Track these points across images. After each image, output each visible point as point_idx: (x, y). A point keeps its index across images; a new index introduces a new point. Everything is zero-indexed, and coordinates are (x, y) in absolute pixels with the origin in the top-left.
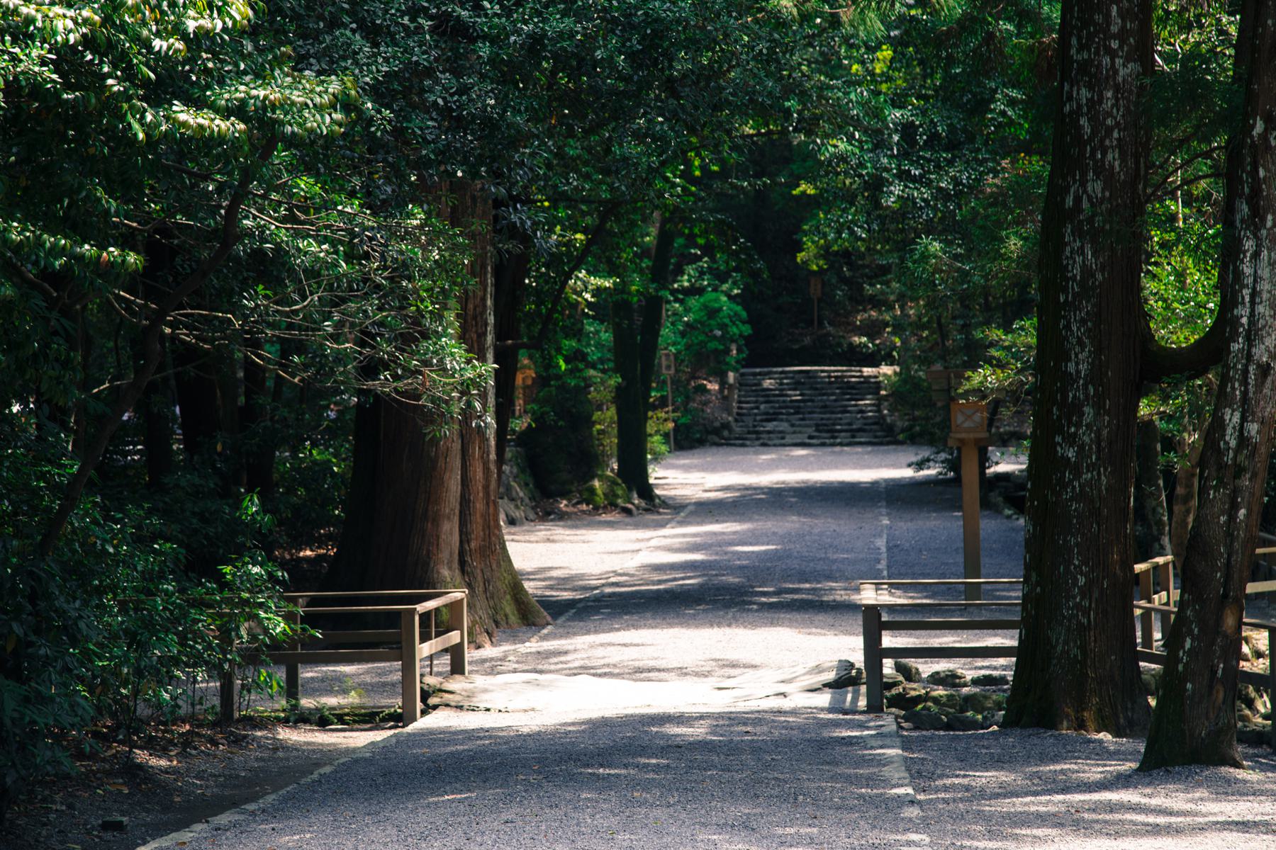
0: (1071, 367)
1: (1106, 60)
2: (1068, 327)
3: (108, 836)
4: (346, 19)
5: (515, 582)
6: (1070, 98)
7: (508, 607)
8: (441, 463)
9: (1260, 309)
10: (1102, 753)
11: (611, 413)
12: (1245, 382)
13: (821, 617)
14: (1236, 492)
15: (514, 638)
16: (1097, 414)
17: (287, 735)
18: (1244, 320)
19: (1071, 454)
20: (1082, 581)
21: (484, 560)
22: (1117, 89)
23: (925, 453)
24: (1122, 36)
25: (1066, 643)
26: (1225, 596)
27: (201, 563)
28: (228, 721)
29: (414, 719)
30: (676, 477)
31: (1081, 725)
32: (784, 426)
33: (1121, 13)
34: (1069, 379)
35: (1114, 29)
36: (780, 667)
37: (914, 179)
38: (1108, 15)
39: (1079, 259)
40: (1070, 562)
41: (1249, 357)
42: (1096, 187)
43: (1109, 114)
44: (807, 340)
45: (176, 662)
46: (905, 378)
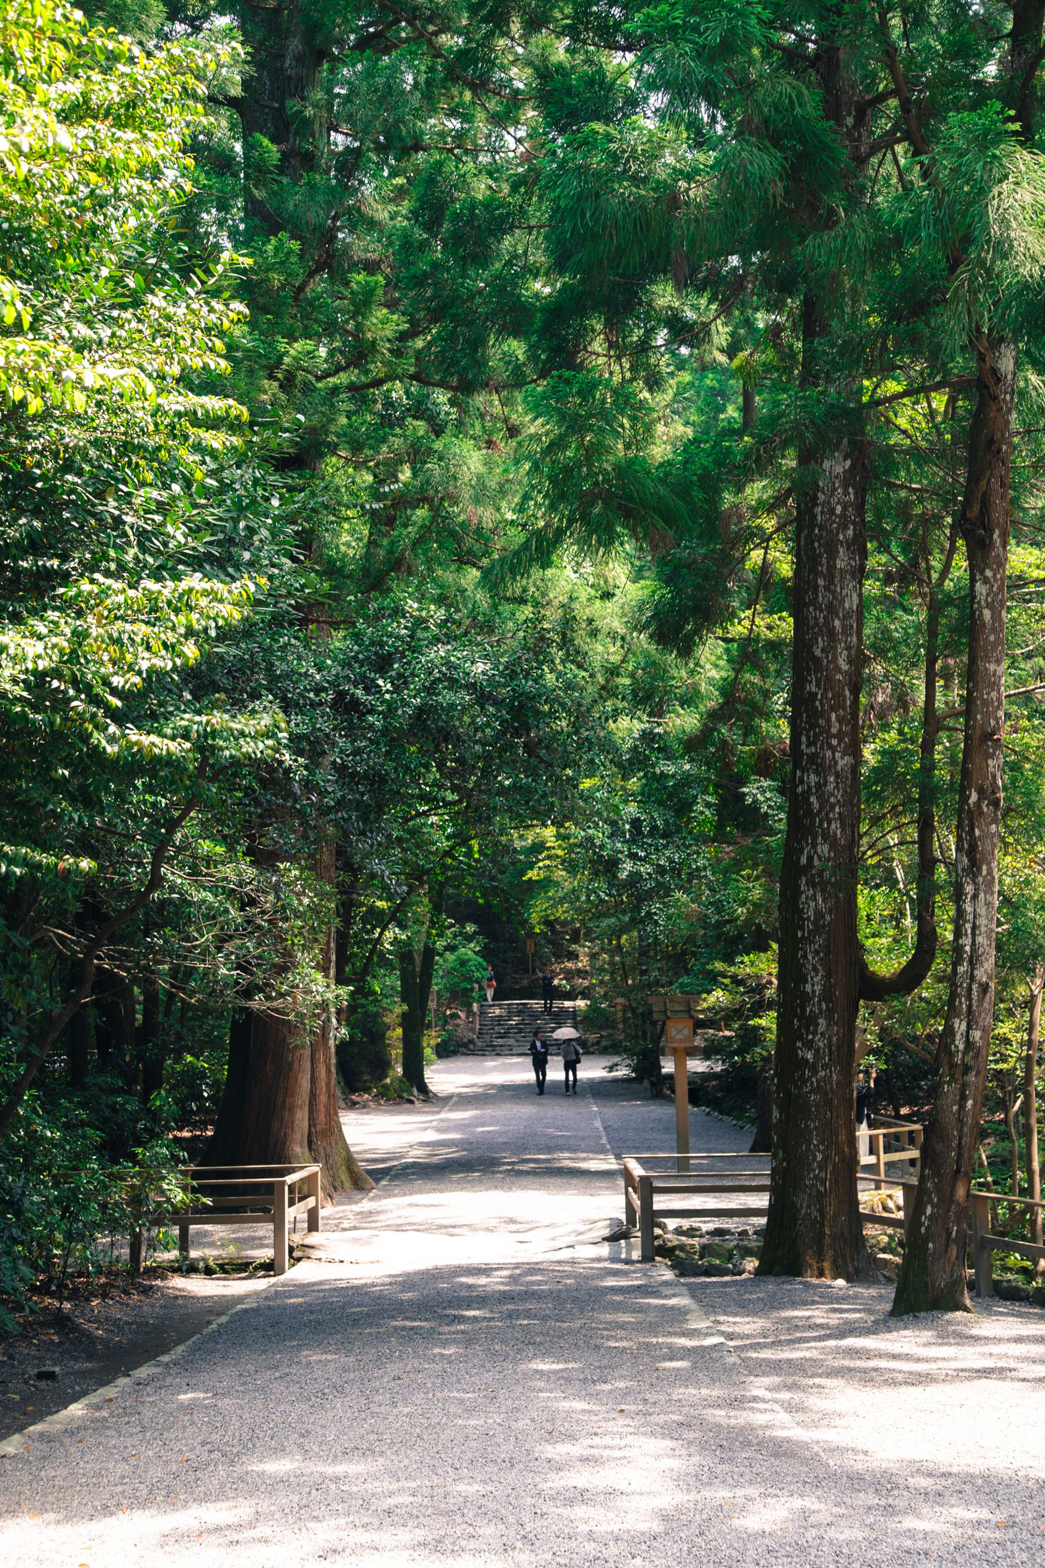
0: (808, 988)
1: (829, 754)
2: (805, 956)
3: (43, 1384)
4: (264, 692)
5: (350, 1161)
6: (802, 781)
7: (344, 1176)
8: (296, 1065)
9: (979, 939)
10: (830, 1298)
11: (399, 1031)
12: (969, 997)
13: (575, 1181)
14: (964, 1086)
15: (351, 1201)
16: (829, 1025)
17: (178, 1283)
18: (968, 948)
19: (809, 1056)
20: (819, 1157)
21: (325, 1138)
22: (837, 775)
23: (616, 1059)
24: (840, 736)
25: (809, 1207)
26: (958, 1171)
27: (117, 1147)
28: (136, 1276)
29: (282, 1272)
30: (443, 1077)
31: (821, 1274)
32: (512, 1042)
33: (838, 720)
34: (806, 998)
35: (834, 731)
36: (555, 1225)
37: (640, 859)
38: (829, 720)
39: (812, 904)
40: (810, 1142)
41: (972, 978)
42: (823, 849)
43: (832, 794)
44: (525, 982)
45: (98, 1227)
46: (593, 1008)
